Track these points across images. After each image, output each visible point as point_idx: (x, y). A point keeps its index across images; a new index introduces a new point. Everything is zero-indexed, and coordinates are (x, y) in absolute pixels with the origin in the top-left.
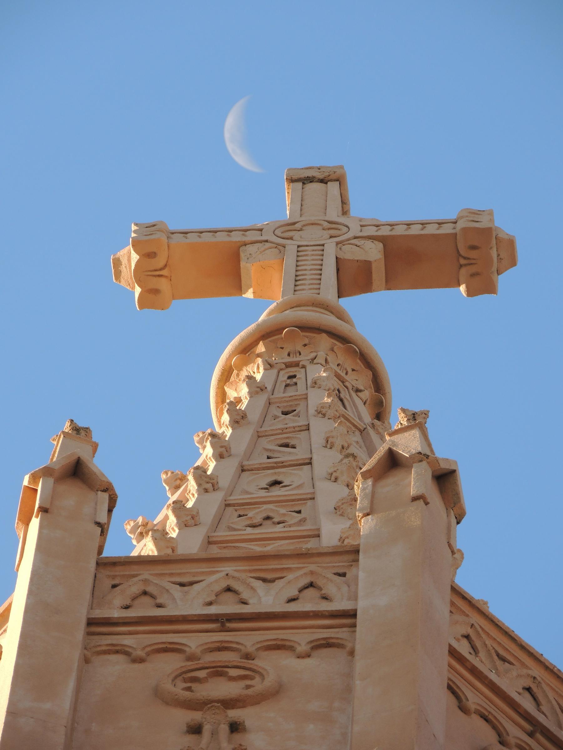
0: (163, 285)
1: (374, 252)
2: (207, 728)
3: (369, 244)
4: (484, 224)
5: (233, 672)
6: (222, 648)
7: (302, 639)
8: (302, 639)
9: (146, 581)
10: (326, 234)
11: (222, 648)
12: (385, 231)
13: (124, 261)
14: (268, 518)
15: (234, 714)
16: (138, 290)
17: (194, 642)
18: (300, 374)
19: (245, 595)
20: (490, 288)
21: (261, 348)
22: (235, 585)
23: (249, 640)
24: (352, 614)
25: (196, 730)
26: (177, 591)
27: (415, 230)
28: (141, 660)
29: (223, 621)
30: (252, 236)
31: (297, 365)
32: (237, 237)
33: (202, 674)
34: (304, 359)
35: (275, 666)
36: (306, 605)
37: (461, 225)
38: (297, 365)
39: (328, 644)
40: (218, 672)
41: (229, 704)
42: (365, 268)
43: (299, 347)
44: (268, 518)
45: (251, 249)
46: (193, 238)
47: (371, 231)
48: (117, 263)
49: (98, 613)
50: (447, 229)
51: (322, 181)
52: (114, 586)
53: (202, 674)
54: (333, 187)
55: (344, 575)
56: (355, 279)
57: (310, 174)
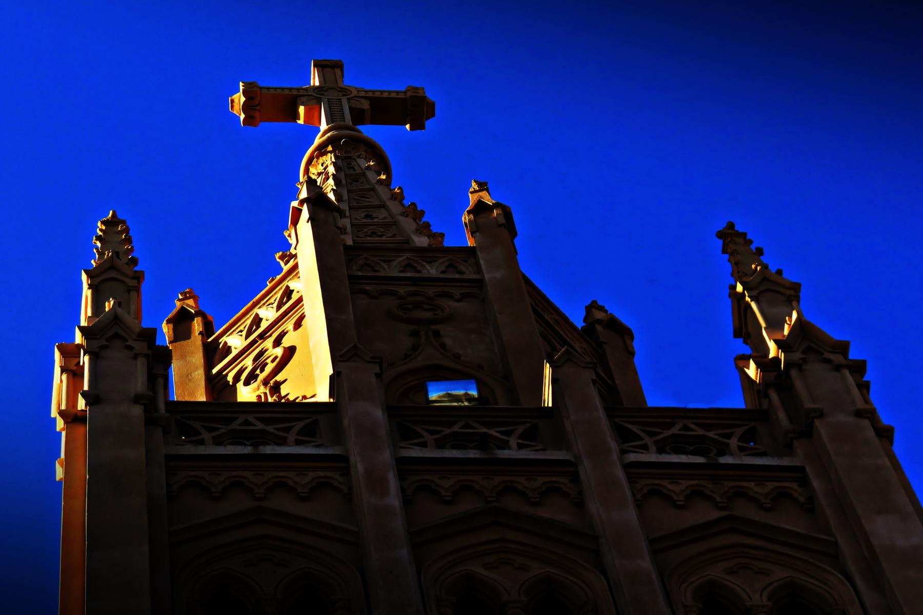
0: (257, 114)
1: (366, 105)
3: (363, 101)
4: (421, 94)
5: (426, 307)
7: (457, 293)
8: (457, 293)
10: (341, 94)
12: (370, 94)
13: (236, 101)
14: (373, 233)
16: (242, 116)
17: (402, 291)
18: (354, 163)
19: (419, 268)
20: (422, 127)
21: (330, 148)
23: (431, 291)
25: (415, 334)
26: (385, 265)
27: (385, 95)
29: (414, 281)
30: (301, 93)
32: (295, 92)
33: (410, 306)
34: (354, 154)
37: (409, 94)
42: (362, 111)
45: (304, 99)
46: (272, 91)
47: (363, 94)
48: (233, 101)
50: (401, 96)
53: (410, 306)
56: (359, 117)
57: (325, 63)
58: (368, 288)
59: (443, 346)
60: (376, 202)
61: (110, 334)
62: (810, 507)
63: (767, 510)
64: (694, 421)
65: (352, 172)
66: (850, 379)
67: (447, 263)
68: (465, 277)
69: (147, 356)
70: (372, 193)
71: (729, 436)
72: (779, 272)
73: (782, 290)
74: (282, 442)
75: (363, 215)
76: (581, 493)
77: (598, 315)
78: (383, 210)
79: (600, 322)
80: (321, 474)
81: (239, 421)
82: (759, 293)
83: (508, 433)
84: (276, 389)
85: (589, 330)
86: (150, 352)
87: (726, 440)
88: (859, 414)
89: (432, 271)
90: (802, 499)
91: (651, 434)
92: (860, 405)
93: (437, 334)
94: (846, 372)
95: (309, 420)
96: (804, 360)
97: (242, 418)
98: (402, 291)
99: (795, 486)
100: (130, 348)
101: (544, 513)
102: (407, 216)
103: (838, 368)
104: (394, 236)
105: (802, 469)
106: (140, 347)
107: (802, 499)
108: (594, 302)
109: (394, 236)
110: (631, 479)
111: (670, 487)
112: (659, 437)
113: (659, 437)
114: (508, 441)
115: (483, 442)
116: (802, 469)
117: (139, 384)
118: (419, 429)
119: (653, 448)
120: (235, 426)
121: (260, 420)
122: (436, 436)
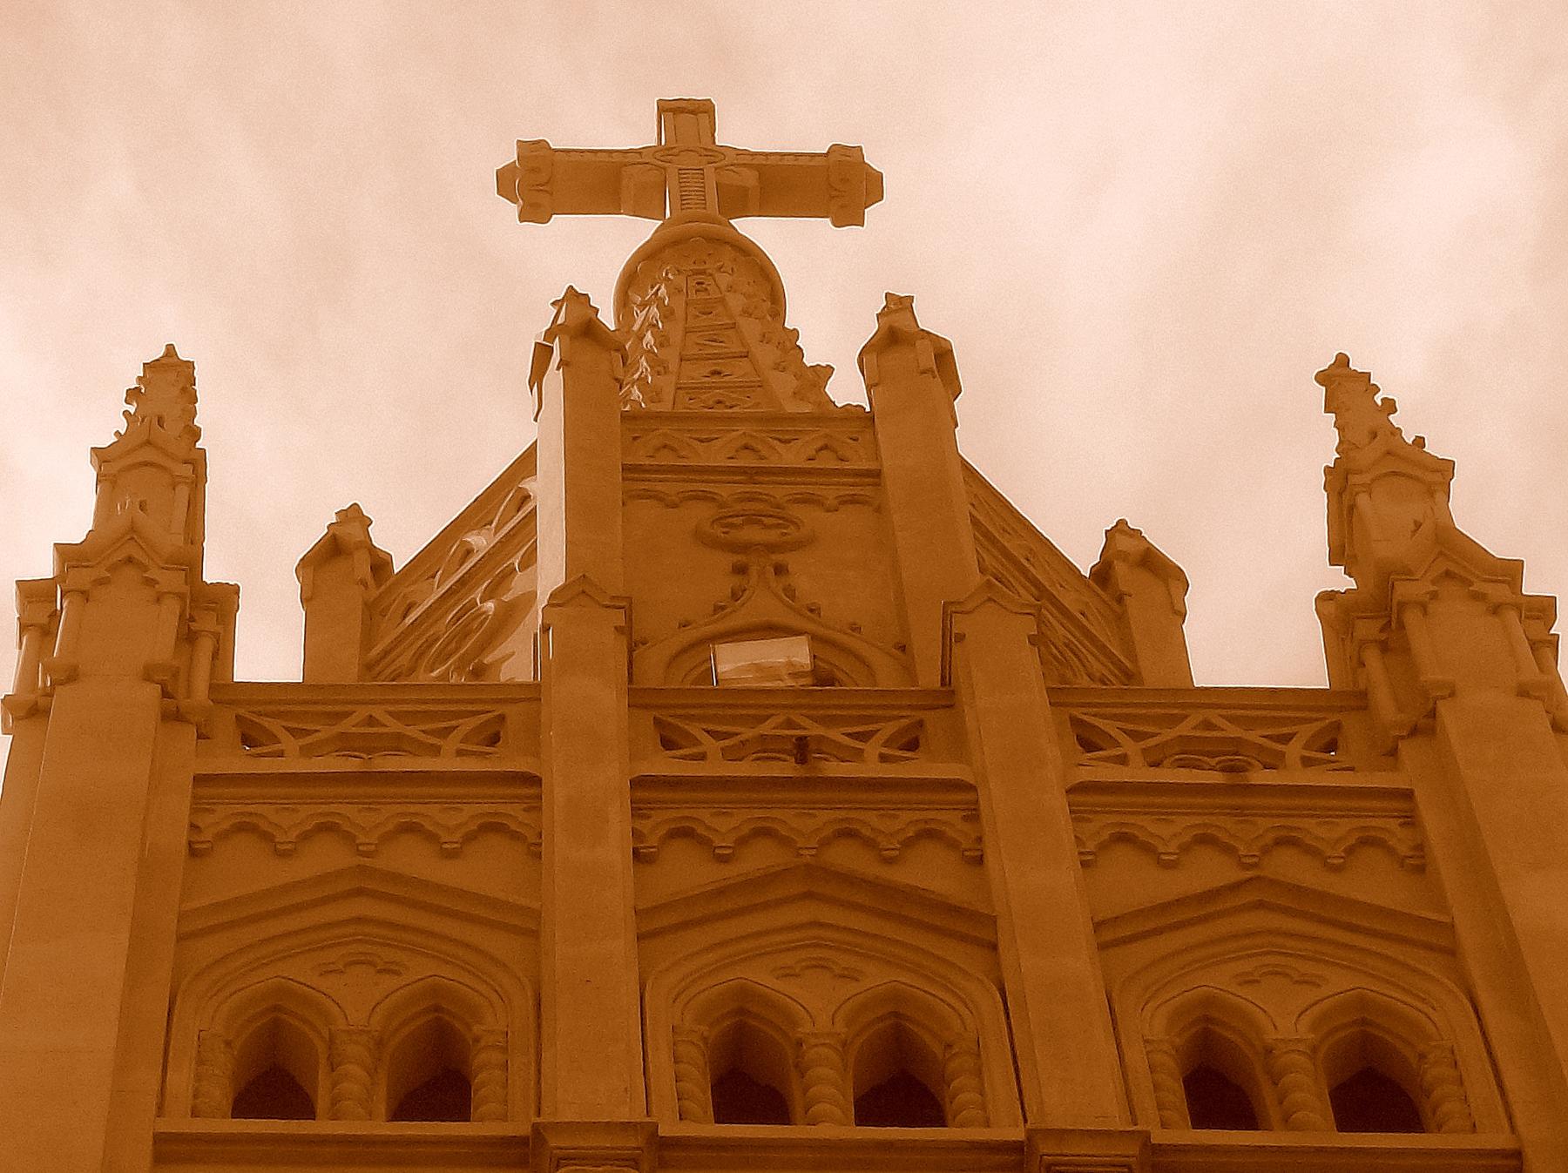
1: (750, 179)
2: (754, 570)
6: (751, 499)
7: (830, 494)
8: (830, 494)
9: (665, 435)
11: (751, 499)
14: (719, 402)
15: (777, 558)
17: (724, 491)
18: (708, 281)
22: (752, 443)
23: (780, 493)
24: (877, 474)
25: (740, 570)
28: (675, 506)
29: (751, 474)
31: (703, 272)
34: (709, 266)
35: (809, 517)
36: (828, 462)
38: (703, 272)
39: (853, 500)
40: (753, 519)
41: (771, 548)
42: (744, 191)
43: (705, 257)
44: (719, 402)
47: (747, 160)
49: (630, 461)
50: (821, 161)
51: (692, 112)
52: (635, 439)
53: (739, 520)
54: (704, 118)
55: (856, 440)
57: (683, 104)
58: (659, 487)
59: (790, 592)
60: (736, 348)
61: (121, 555)
62: (1418, 864)
63: (1336, 869)
64: (1224, 712)
65: (702, 295)
66: (1518, 630)
67: (820, 444)
68: (847, 466)
69: (181, 596)
70: (730, 332)
71: (1286, 739)
72: (1420, 442)
73: (1418, 473)
74: (435, 751)
75: (706, 372)
76: (980, 839)
77: (1123, 543)
78: (744, 363)
79: (1123, 556)
80: (486, 808)
81: (354, 719)
82: (1373, 480)
83: (863, 737)
84: (478, 672)
85: (1102, 573)
86: (186, 589)
87: (1279, 747)
88: (1523, 692)
89: (790, 456)
90: (1403, 850)
91: (1136, 736)
92: (1530, 672)
93: (780, 570)
94: (1512, 616)
95: (484, 717)
96: (1434, 596)
97: (362, 712)
98: (724, 491)
99: (1393, 824)
100: (151, 582)
101: (902, 875)
102: (784, 370)
103: (1496, 610)
104: (757, 405)
105: (1408, 795)
106: (172, 581)
107: (1403, 850)
108: (1122, 522)
109: (757, 405)
110: (1077, 815)
111: (1152, 828)
112: (1151, 742)
113: (1151, 742)
114: (862, 750)
115: (802, 749)
116: (1408, 795)
117: (160, 643)
118: (695, 730)
119: (1136, 759)
120: (346, 726)
121: (397, 716)
122: (727, 742)
